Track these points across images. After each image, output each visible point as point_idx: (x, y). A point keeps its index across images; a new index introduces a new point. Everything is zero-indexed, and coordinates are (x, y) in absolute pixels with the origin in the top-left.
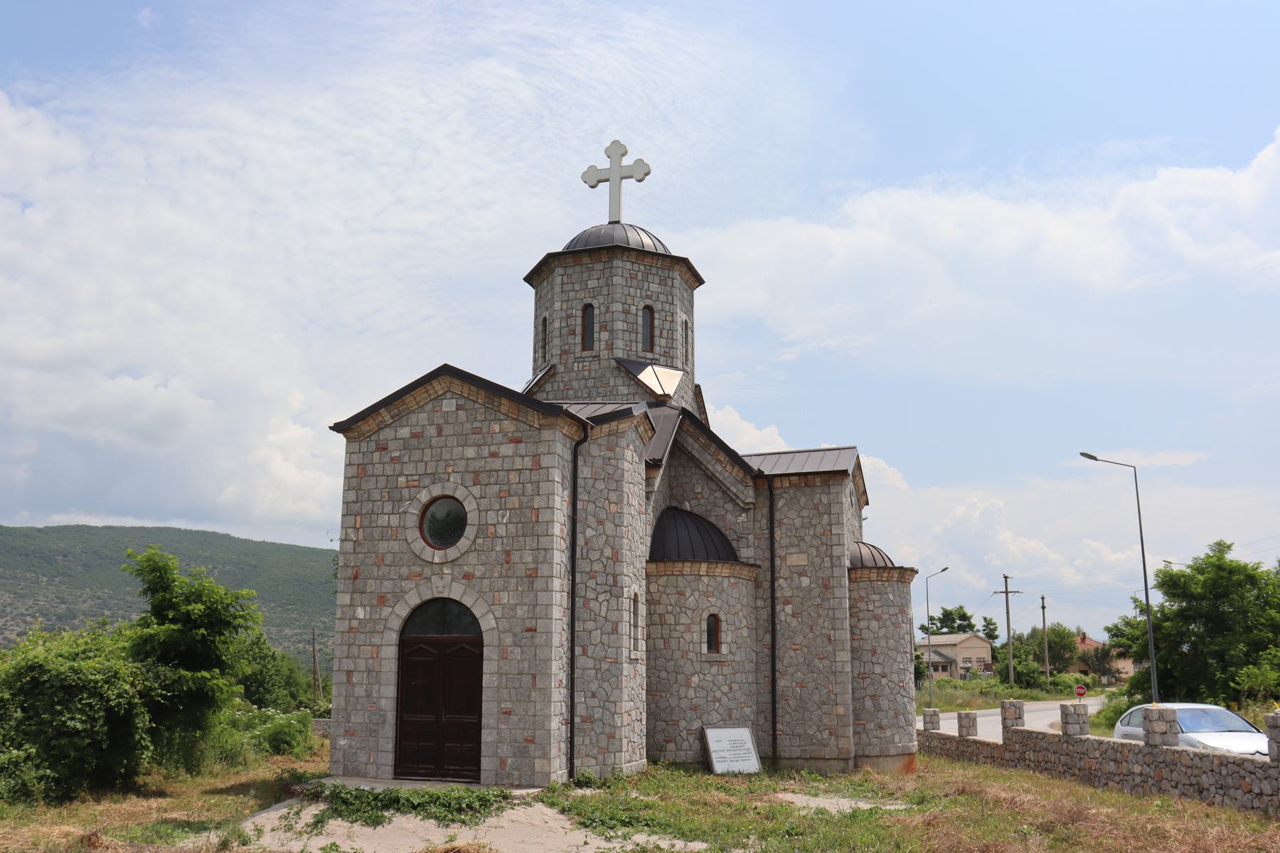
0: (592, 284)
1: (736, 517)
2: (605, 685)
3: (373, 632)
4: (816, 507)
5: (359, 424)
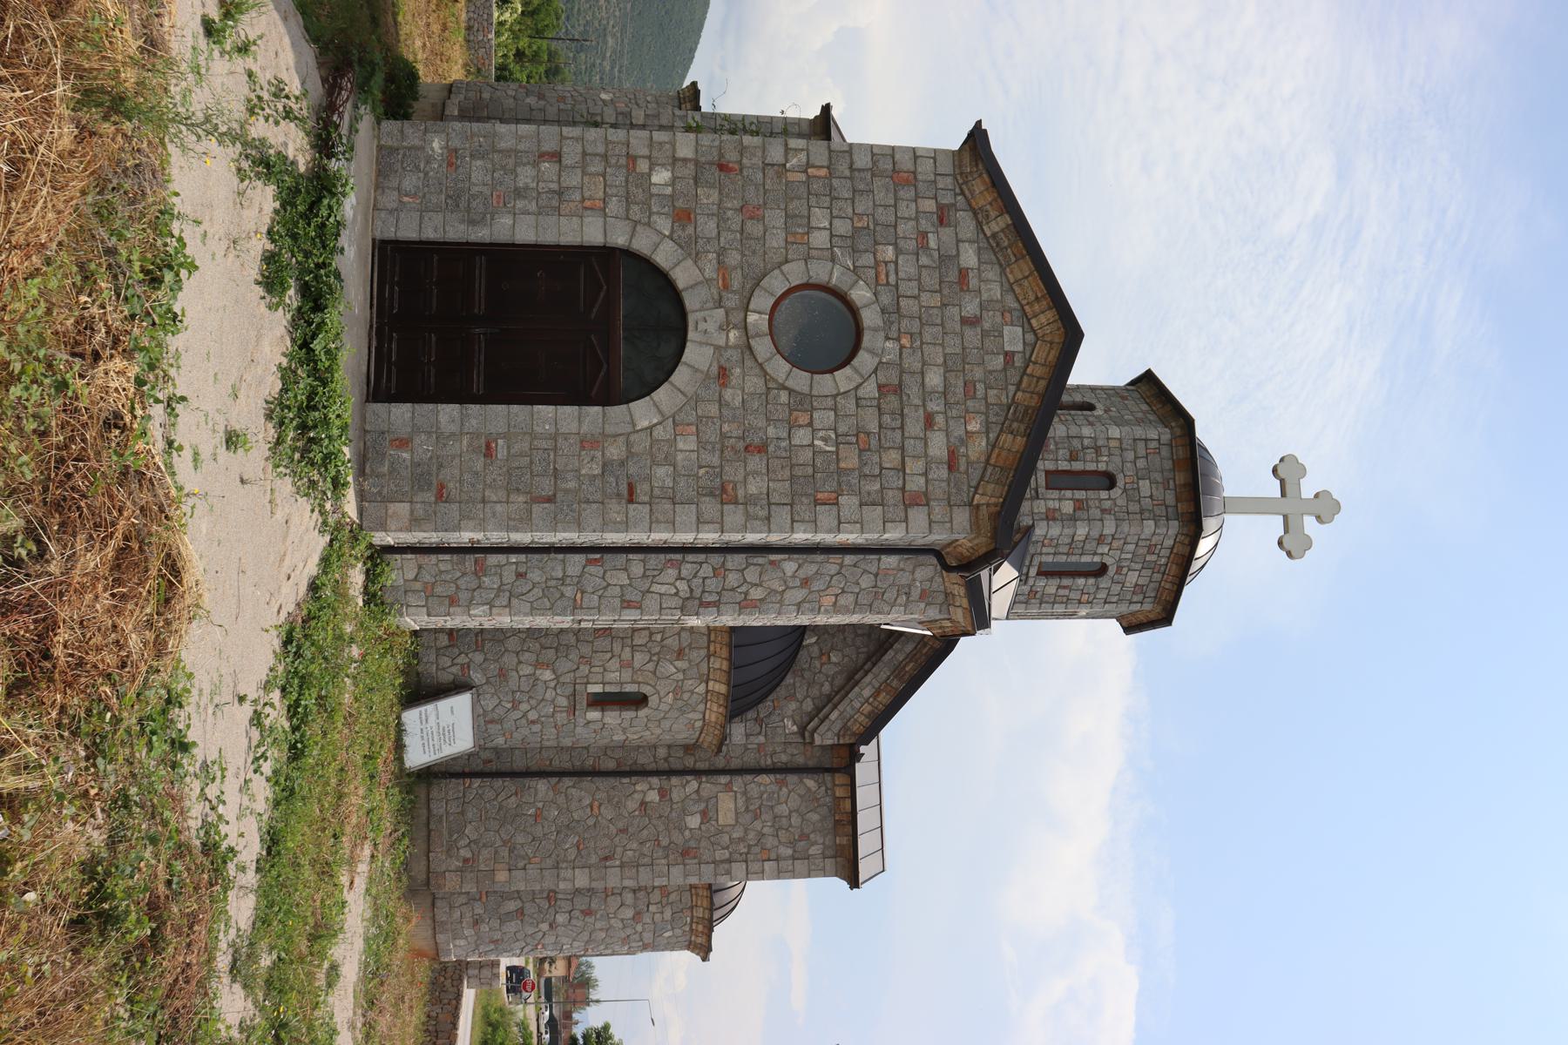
0: (1145, 486)
1: (792, 716)
2: (537, 592)
3: (628, 200)
4: (804, 836)
5: (985, 176)
